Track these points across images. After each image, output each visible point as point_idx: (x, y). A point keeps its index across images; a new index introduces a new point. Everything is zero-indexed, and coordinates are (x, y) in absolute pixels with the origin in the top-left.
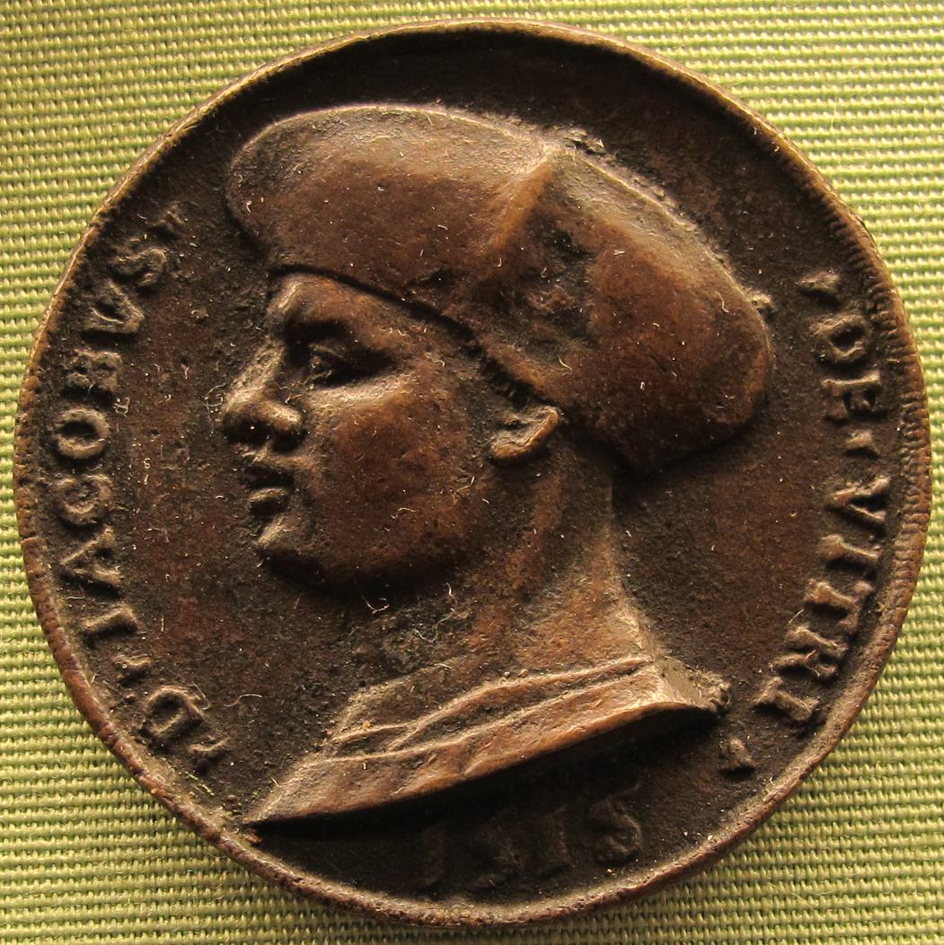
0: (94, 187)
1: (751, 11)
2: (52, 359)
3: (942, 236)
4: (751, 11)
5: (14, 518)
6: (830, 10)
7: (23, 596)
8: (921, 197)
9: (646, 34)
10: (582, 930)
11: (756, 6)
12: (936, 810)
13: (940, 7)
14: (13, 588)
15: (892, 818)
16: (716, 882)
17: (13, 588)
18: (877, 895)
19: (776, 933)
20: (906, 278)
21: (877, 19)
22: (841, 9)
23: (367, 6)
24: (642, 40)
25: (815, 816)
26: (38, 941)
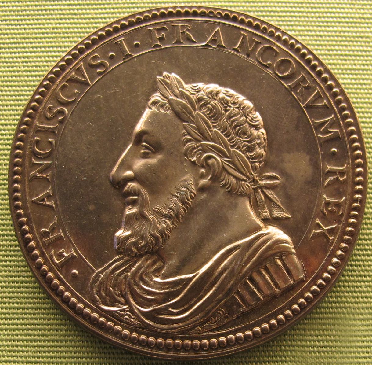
0: (26, 85)
1: (9, 4)
2: (11, 160)
3: (371, 328)
4: (9, 4)
5: (10, 147)
6: (17, 4)
7: (8, 215)
8: (362, 91)
9: (258, 11)
10: (234, 362)
11: (10, 2)
12: (369, 316)
13: (370, 2)
14: (5, 212)
15: (357, 255)
16: (291, 350)
17: (5, 212)
18: (354, 277)
19: (290, 349)
20: (366, 125)
21: (360, 354)
22: (32, 3)
23: (42, 2)
24: (256, 13)
25: (327, 305)
26: (56, 364)
